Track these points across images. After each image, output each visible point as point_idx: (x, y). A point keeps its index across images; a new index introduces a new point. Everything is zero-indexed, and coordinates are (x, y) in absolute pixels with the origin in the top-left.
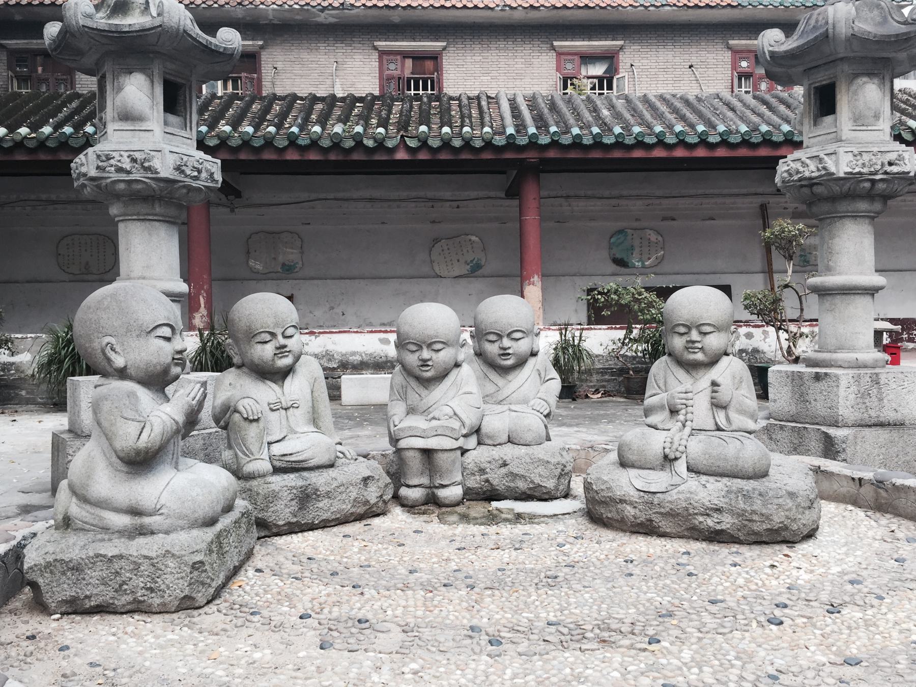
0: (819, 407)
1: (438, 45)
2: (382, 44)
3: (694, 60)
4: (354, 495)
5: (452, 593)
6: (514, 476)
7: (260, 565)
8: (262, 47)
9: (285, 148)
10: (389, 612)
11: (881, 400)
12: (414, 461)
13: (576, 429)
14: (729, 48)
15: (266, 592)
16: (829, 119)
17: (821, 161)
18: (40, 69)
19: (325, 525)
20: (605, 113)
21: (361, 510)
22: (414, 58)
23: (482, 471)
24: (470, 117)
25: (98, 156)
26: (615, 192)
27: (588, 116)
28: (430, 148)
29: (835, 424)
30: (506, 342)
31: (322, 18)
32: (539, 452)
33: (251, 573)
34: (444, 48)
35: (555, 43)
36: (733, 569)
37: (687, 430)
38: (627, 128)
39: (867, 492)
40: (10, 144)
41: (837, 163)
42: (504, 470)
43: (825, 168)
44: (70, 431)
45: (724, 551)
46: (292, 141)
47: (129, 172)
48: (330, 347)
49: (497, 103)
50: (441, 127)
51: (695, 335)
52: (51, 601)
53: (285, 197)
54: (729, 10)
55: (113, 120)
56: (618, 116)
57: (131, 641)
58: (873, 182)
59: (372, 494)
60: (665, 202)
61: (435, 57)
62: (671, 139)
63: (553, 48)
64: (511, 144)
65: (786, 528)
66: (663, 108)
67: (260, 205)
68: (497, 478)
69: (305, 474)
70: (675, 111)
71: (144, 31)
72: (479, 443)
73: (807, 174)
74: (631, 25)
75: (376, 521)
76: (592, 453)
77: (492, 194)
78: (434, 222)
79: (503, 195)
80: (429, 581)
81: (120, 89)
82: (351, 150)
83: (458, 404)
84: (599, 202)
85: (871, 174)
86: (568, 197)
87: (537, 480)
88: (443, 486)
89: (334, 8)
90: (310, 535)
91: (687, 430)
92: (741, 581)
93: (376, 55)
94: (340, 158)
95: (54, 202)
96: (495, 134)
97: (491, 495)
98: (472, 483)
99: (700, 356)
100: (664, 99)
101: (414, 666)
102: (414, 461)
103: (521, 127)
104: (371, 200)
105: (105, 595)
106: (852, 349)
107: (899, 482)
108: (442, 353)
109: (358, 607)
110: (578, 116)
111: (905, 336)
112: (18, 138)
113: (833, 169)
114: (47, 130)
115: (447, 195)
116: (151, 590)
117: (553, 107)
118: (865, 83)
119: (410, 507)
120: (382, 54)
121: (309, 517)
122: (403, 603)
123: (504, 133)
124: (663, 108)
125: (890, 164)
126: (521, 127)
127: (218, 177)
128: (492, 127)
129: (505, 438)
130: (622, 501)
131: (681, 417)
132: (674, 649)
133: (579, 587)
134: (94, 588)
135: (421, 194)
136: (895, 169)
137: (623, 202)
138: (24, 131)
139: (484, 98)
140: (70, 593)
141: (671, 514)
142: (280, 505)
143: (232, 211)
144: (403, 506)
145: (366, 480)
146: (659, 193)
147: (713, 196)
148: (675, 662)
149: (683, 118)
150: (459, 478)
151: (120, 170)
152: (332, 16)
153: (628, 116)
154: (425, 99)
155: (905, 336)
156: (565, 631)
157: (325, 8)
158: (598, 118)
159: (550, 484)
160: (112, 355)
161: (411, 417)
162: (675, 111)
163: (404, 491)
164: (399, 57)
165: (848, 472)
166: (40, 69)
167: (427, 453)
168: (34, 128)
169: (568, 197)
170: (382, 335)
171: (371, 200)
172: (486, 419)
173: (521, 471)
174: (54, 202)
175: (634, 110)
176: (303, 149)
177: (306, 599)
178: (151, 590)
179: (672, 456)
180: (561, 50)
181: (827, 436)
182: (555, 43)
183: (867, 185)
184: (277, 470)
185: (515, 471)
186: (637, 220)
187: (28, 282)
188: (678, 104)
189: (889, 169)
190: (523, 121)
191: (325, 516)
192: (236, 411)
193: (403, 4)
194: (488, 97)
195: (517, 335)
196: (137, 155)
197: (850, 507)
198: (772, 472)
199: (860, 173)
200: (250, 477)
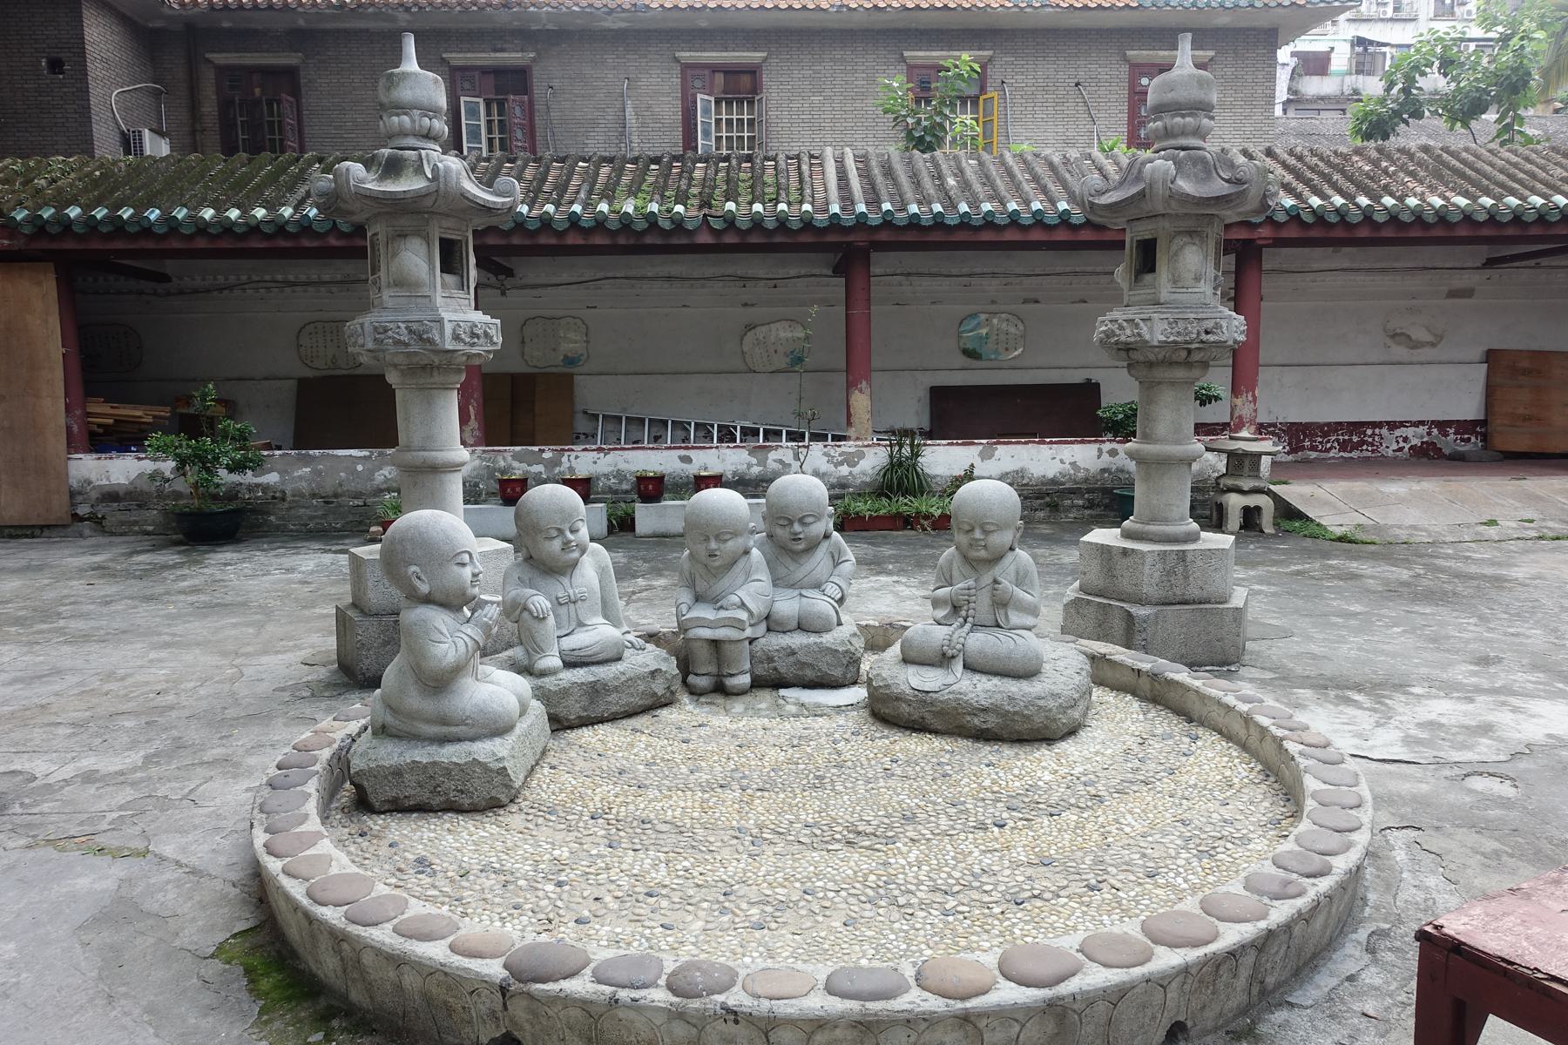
0: (1125, 584)
1: (756, 56)
2: (686, 55)
3: (1082, 75)
4: (641, 688)
5: (729, 795)
6: (803, 665)
7: (555, 762)
8: (534, 60)
9: (566, 230)
10: (670, 813)
11: (1186, 578)
12: (703, 653)
13: (895, 578)
14: (1125, 59)
15: (561, 791)
16: (1148, 278)
17: (1137, 326)
18: (257, 91)
19: (613, 718)
20: (951, 182)
21: (649, 702)
22: (725, 73)
23: (770, 659)
24: (787, 189)
25: (376, 329)
26: (965, 270)
27: (929, 186)
28: (739, 230)
29: (1140, 602)
30: (797, 527)
31: (609, 24)
32: (827, 639)
33: (546, 770)
34: (765, 59)
35: (906, 54)
36: (986, 769)
37: (968, 626)
38: (974, 203)
39: (1145, 684)
40: (244, 229)
41: (1151, 330)
42: (791, 659)
43: (1139, 335)
44: (354, 605)
45: (986, 751)
46: (574, 219)
47: (407, 345)
48: (622, 466)
49: (821, 165)
50: (751, 203)
51: (978, 534)
52: (375, 800)
53: (565, 278)
54: (1126, 13)
55: (389, 286)
56: (965, 185)
57: (450, 838)
58: (1189, 351)
59: (659, 687)
60: (1027, 281)
61: (753, 72)
62: (1026, 218)
63: (903, 59)
64: (835, 223)
65: (1046, 727)
66: (1022, 176)
67: (534, 287)
68: (785, 667)
69: (593, 668)
70: (1036, 179)
71: (419, 196)
72: (769, 630)
73: (1123, 338)
74: (1005, 31)
75: (664, 713)
76: (891, 631)
77: (816, 271)
78: (745, 305)
79: (830, 272)
80: (707, 781)
81: (395, 255)
82: (644, 233)
83: (744, 594)
84: (947, 281)
85: (1187, 342)
86: (909, 274)
87: (825, 668)
88: (732, 675)
89: (624, 10)
90: (601, 729)
91: (968, 626)
92: (987, 783)
93: (677, 70)
94: (632, 242)
95: (294, 284)
96: (816, 211)
97: (777, 683)
98: (760, 671)
99: (983, 554)
100: (1025, 162)
101: (686, 864)
102: (703, 653)
103: (847, 199)
104: (669, 278)
105: (424, 796)
106: (1165, 521)
107: (1171, 675)
108: (730, 543)
109: (643, 806)
110: (917, 184)
111: (1307, 444)
112: (253, 222)
113: (1147, 337)
114: (287, 212)
115: (761, 273)
116: (462, 792)
117: (888, 172)
118: (1185, 244)
119: (695, 693)
120: (687, 68)
121: (600, 709)
122: (682, 804)
123: (827, 210)
124: (1022, 176)
125: (1207, 333)
126: (847, 199)
127: (498, 339)
128: (812, 204)
129: (794, 624)
130: (898, 699)
131: (963, 613)
132: (905, 849)
133: (840, 788)
134: (411, 790)
135: (730, 271)
136: (1211, 338)
137: (974, 281)
138: (260, 213)
139: (806, 159)
140: (392, 793)
141: (941, 713)
142: (571, 701)
143: (503, 294)
144: (692, 693)
145: (653, 673)
146: (1019, 270)
147: (1084, 273)
148: (903, 862)
149: (1044, 190)
150: (747, 666)
151: (398, 342)
152: (623, 20)
153: (977, 187)
154: (734, 162)
155: (1307, 444)
156: (818, 832)
157: (612, 11)
158: (942, 187)
159: (837, 673)
160: (418, 583)
161: (701, 606)
162: (1036, 179)
163: (691, 679)
164: (706, 72)
165: (1129, 662)
166: (257, 91)
167: (715, 644)
168: (271, 206)
169: (909, 274)
170: (683, 453)
171: (669, 278)
172: (777, 605)
173: (810, 660)
174: (294, 284)
175: (987, 177)
176: (586, 232)
177: (597, 799)
178: (462, 792)
179: (950, 653)
180: (912, 62)
181: (1129, 614)
182: (906, 54)
183: (1184, 354)
184: (569, 665)
185: (804, 659)
186: (993, 302)
187: (266, 379)
188: (1041, 169)
189: (1204, 337)
190: (851, 193)
191: (614, 709)
192: (525, 609)
193: (712, 5)
194: (812, 157)
195: (810, 520)
196: (415, 326)
197: (1129, 697)
198: (1047, 667)
199: (1175, 342)
200: (543, 674)
